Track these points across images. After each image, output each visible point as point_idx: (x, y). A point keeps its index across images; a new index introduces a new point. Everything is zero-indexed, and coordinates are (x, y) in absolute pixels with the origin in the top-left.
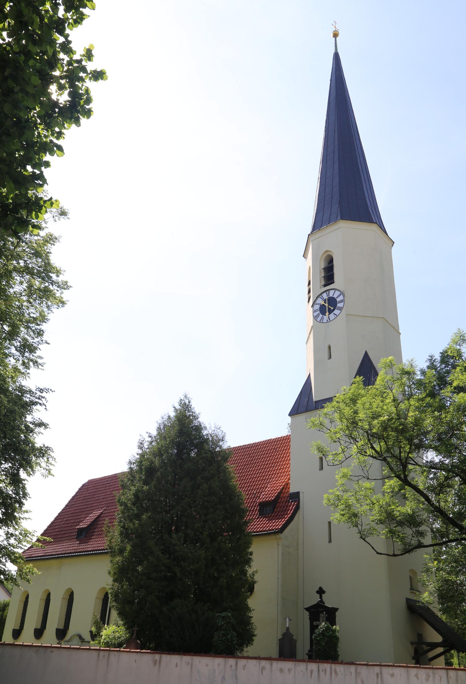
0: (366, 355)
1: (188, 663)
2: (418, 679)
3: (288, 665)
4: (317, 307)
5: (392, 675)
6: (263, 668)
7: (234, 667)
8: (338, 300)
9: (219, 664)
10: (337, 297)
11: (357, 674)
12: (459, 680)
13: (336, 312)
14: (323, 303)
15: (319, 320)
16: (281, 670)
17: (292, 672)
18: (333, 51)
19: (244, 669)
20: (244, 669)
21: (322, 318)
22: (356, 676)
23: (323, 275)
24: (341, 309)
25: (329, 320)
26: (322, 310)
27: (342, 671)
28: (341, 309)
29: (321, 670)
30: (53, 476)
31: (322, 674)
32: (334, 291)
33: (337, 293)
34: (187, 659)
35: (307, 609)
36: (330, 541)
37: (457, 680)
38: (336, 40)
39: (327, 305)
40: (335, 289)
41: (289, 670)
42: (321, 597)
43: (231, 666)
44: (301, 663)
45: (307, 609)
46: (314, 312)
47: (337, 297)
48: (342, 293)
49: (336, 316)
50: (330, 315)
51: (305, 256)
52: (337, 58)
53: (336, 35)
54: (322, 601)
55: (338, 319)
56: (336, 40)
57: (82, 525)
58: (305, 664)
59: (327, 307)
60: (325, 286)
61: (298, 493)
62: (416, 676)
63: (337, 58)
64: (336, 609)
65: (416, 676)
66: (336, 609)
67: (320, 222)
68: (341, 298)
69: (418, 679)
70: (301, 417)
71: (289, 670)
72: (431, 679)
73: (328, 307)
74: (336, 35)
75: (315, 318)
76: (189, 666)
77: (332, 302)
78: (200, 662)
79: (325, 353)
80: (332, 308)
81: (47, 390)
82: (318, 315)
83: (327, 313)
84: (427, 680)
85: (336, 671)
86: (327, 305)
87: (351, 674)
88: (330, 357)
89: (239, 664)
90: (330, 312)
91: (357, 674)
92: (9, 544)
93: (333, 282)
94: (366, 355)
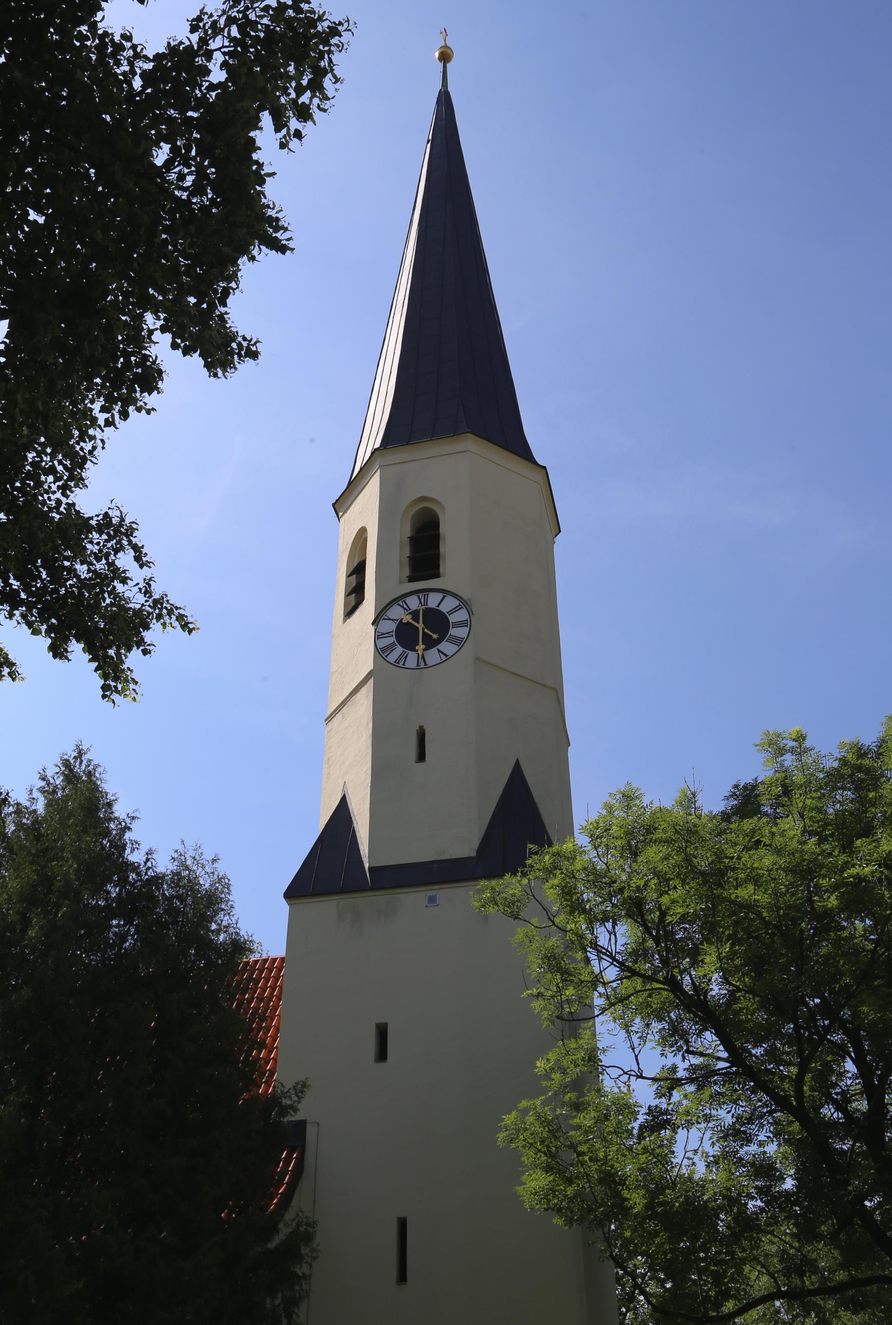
0: (517, 773)
4: (392, 627)
8: (452, 618)
10: (452, 612)
13: (446, 647)
14: (408, 619)
15: (392, 658)
18: (439, 86)
21: (403, 657)
23: (407, 553)
24: (459, 642)
26: (406, 636)
28: (459, 642)
30: (186, 626)
32: (440, 596)
36: (402, 1277)
38: (445, 67)
39: (420, 626)
40: (445, 592)
46: (378, 636)
47: (452, 612)
48: (464, 604)
49: (444, 658)
50: (426, 653)
51: (340, 505)
52: (445, 102)
53: (445, 57)
55: (447, 671)
56: (445, 67)
59: (413, 634)
60: (411, 579)
63: (445, 102)
67: (402, 430)
68: (462, 615)
70: (325, 909)
73: (424, 632)
74: (445, 57)
75: (381, 652)
77: (438, 624)
79: (404, 747)
80: (435, 636)
81: (204, 8)
82: (389, 648)
83: (421, 647)
86: (420, 626)
88: (421, 757)
90: (430, 644)
92: (708, 1118)
93: (437, 575)
94: (517, 773)
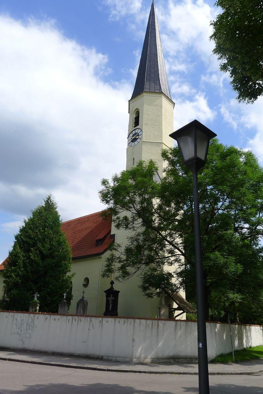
1: (12, 316)
2: (120, 323)
3: (111, 320)
5: (107, 322)
6: (47, 318)
7: (33, 318)
9: (26, 316)
11: (91, 321)
12: (141, 323)
16: (55, 319)
17: (60, 320)
18: (152, 2)
19: (37, 319)
20: (37, 319)
21: (132, 144)
22: (90, 323)
25: (135, 145)
27: (84, 319)
29: (73, 319)
31: (74, 321)
33: (140, 130)
34: (11, 314)
35: (105, 292)
37: (140, 324)
41: (59, 319)
42: (112, 286)
43: (32, 318)
44: (65, 316)
45: (105, 292)
54: (112, 287)
57: (98, 238)
58: (66, 316)
60: (135, 127)
61: (114, 235)
62: (119, 322)
64: (119, 292)
65: (119, 322)
66: (119, 292)
69: (120, 323)
71: (59, 319)
72: (126, 323)
75: (129, 144)
76: (13, 317)
78: (17, 315)
84: (124, 324)
85: (80, 320)
87: (88, 321)
89: (35, 316)
91: (91, 321)
